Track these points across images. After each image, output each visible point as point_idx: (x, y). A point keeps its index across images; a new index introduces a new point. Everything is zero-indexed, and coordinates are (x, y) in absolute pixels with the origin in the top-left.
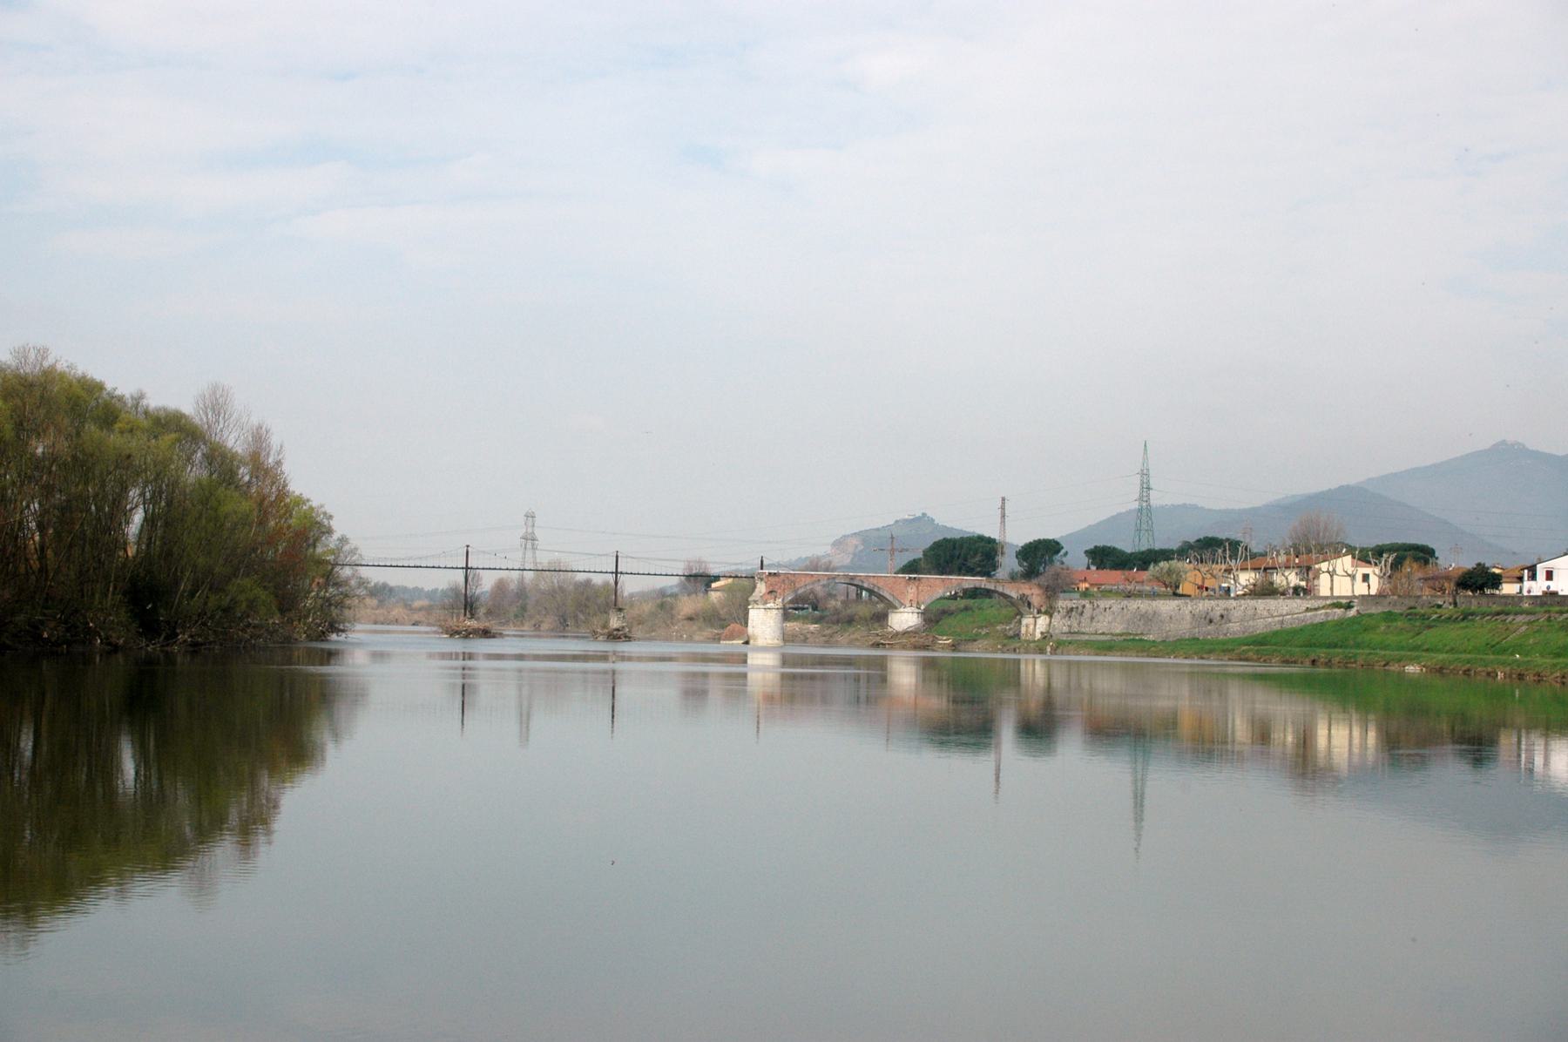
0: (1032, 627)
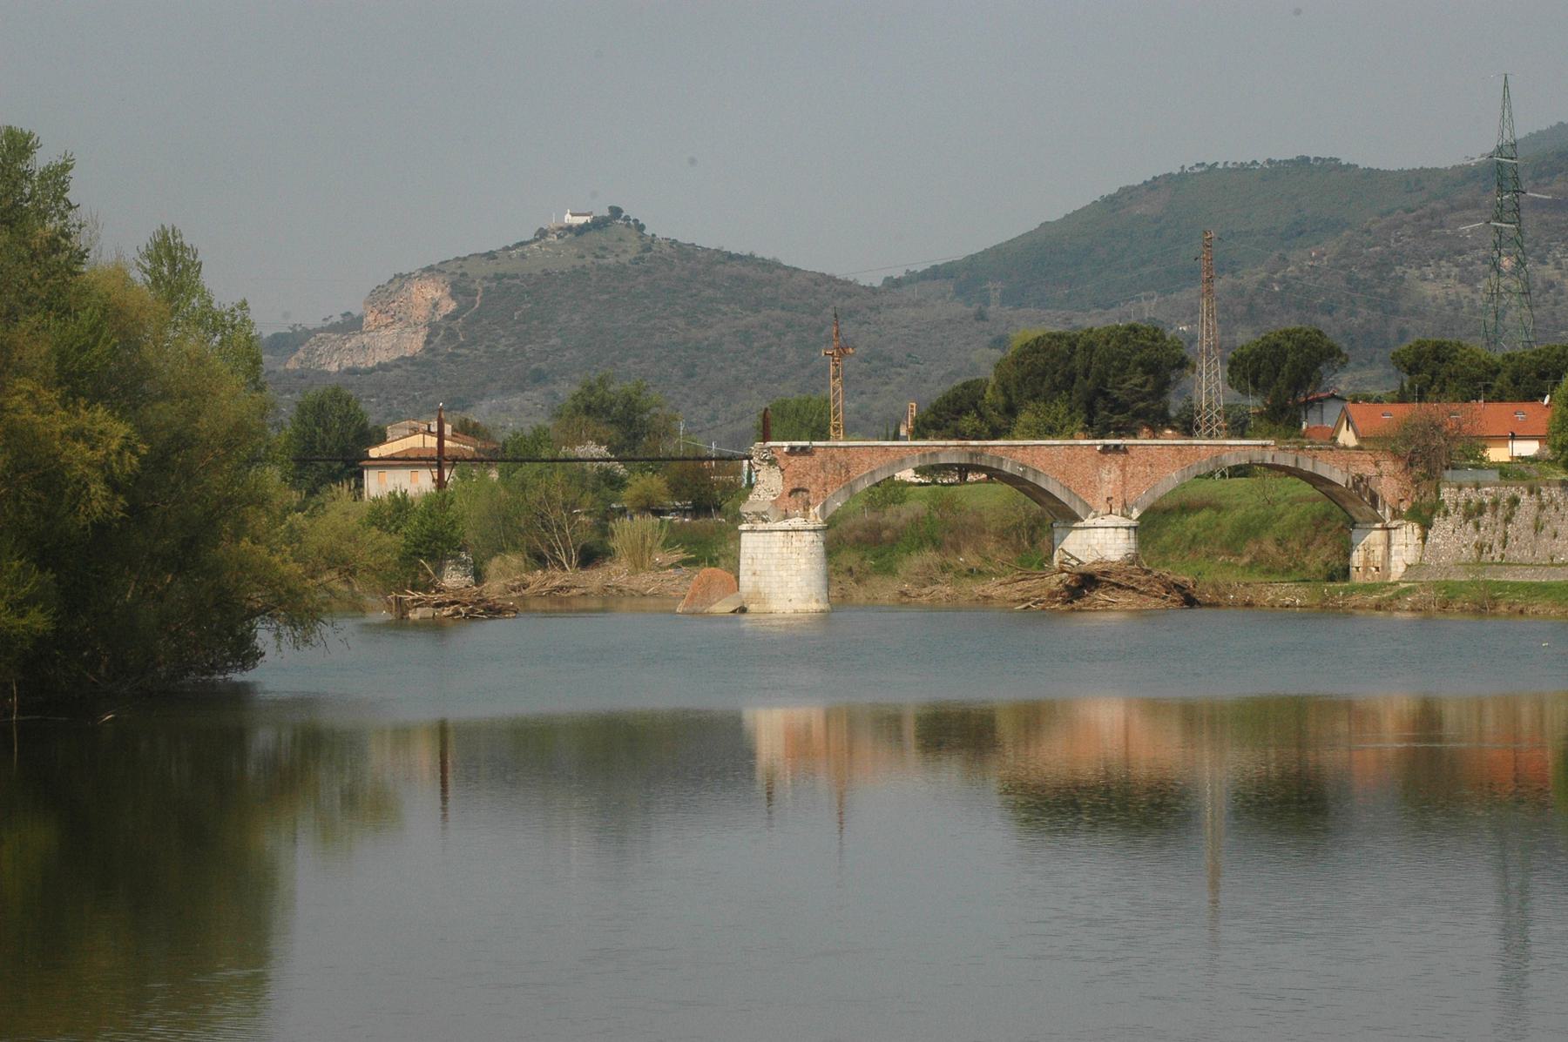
0: (1379, 551)
